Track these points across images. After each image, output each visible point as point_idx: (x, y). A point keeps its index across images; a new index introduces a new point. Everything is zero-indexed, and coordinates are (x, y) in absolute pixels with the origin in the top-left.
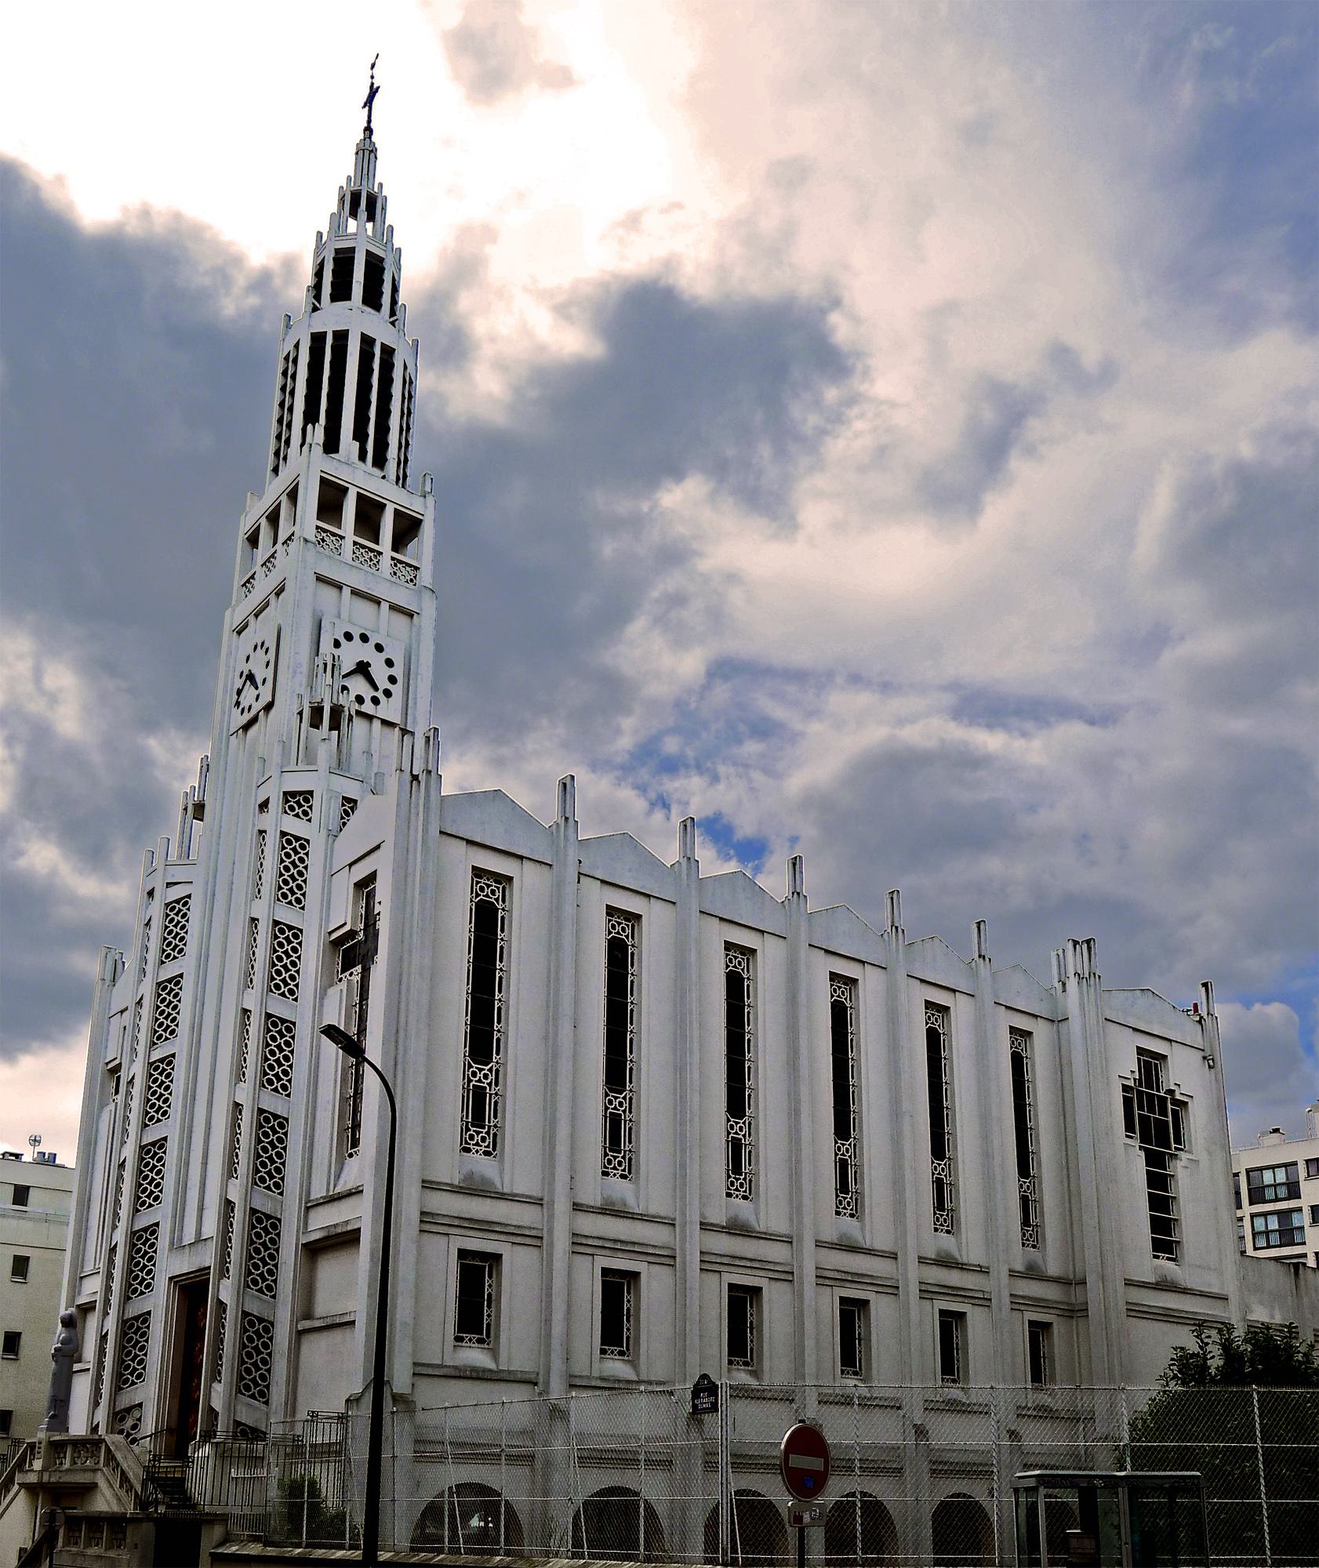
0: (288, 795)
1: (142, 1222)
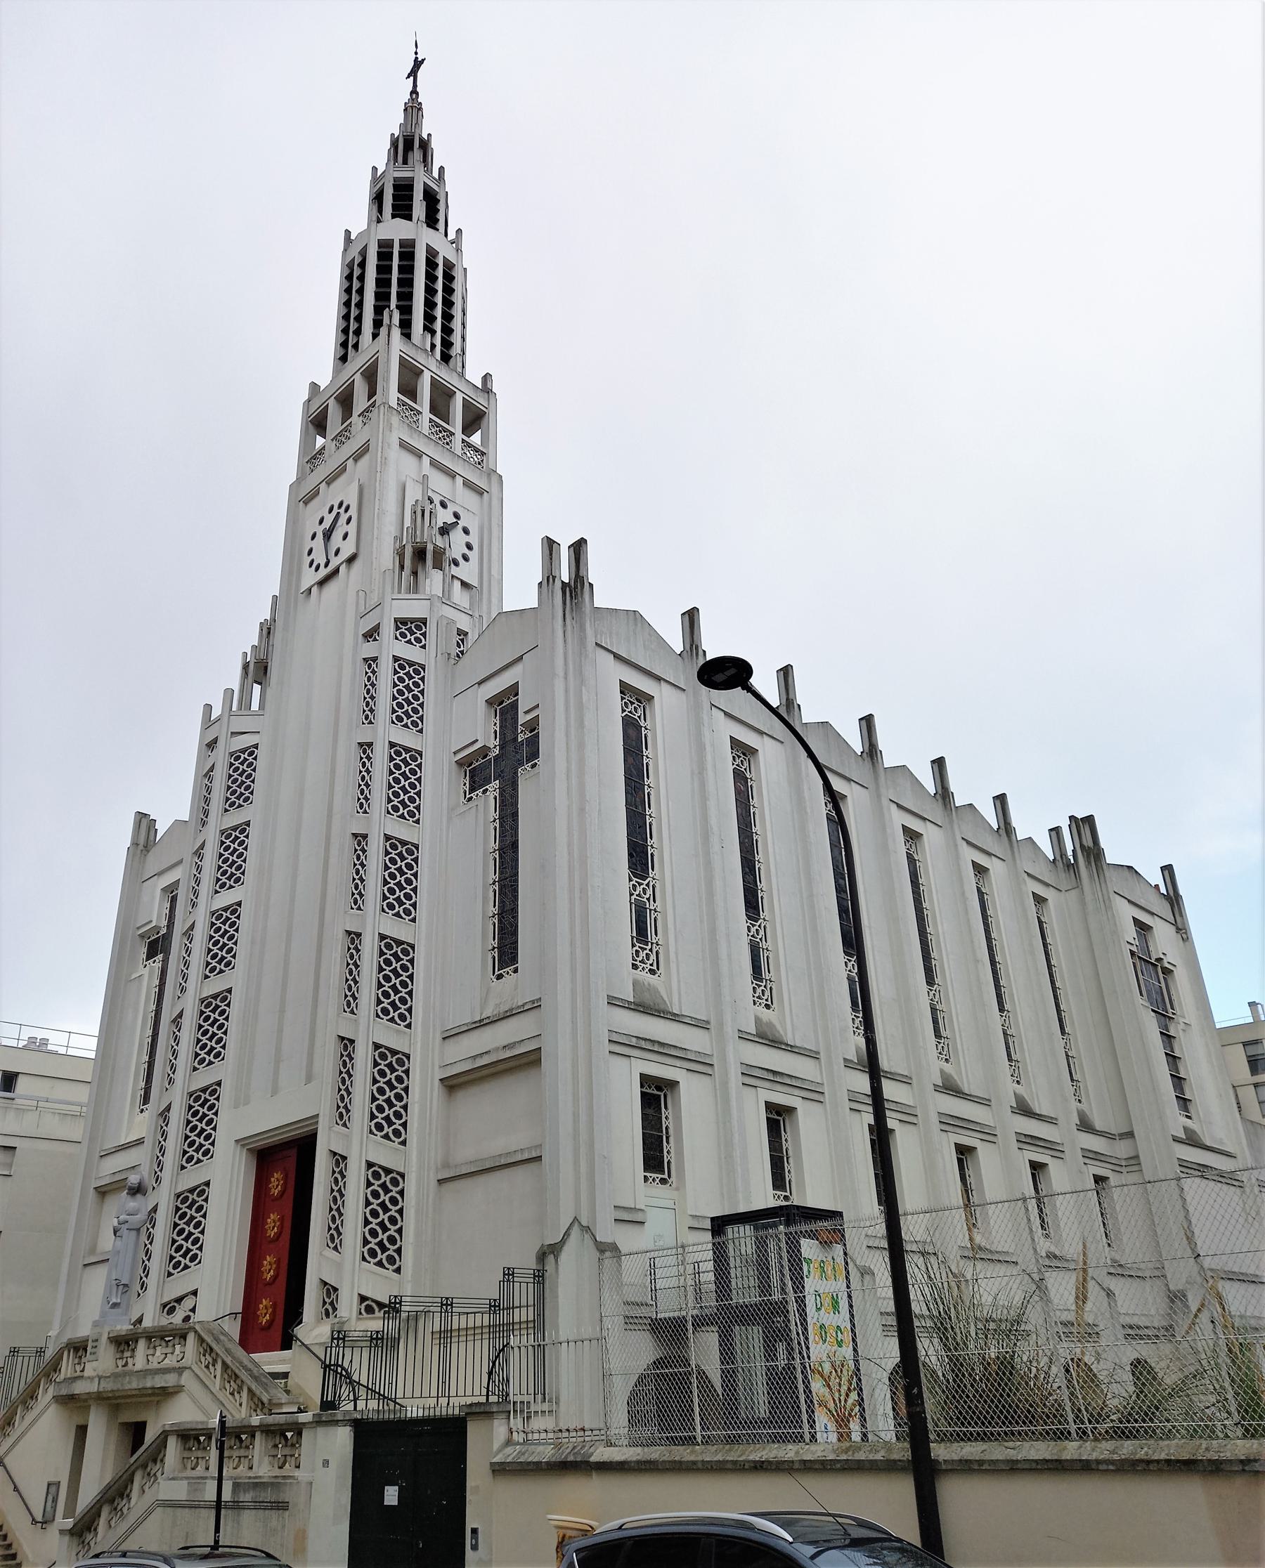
0: (400, 622)
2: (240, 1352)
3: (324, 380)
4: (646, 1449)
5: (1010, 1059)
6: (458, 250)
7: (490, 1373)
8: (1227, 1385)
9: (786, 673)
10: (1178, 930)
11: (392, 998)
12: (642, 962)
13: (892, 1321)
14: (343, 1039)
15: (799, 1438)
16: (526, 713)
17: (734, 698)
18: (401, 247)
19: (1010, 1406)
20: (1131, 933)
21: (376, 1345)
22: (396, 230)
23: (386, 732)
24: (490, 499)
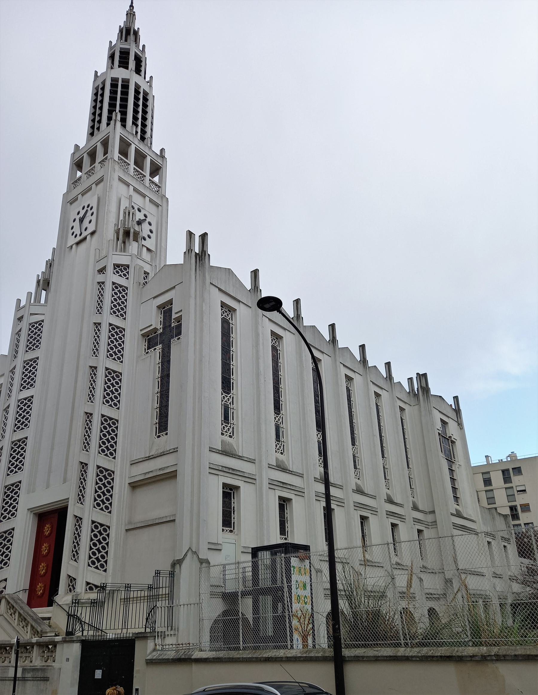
0: (116, 266)
2: (27, 608)
3: (82, 142)
4: (217, 652)
5: (385, 479)
6: (151, 86)
7: (147, 619)
8: (467, 624)
9: (297, 302)
10: (459, 424)
11: (107, 444)
12: (226, 432)
13: (329, 592)
14: (82, 463)
15: (286, 647)
16: (176, 313)
17: (274, 315)
18: (122, 82)
19: (377, 633)
20: (439, 425)
21: (94, 606)
22: (120, 73)
23: (108, 318)
24: (162, 210)
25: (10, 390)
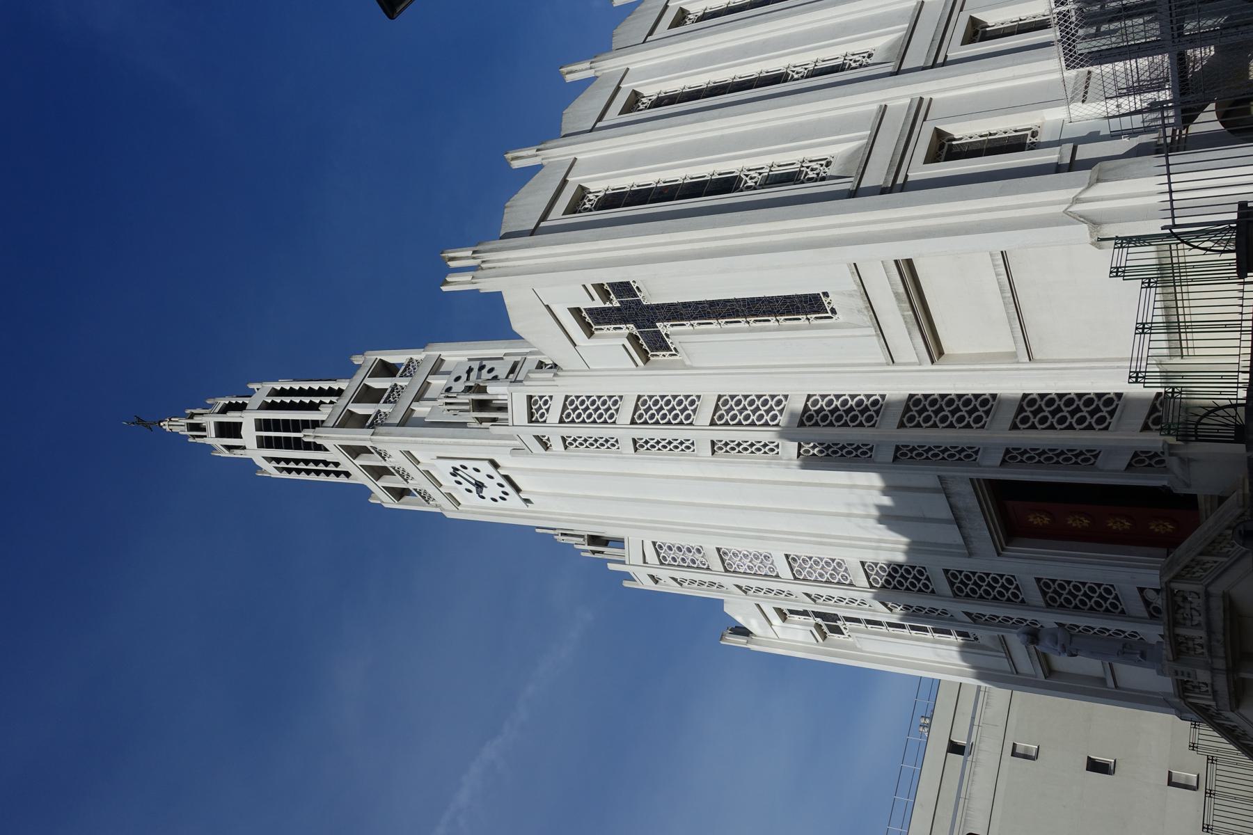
1: (1035, 596)
25: (780, 592)
